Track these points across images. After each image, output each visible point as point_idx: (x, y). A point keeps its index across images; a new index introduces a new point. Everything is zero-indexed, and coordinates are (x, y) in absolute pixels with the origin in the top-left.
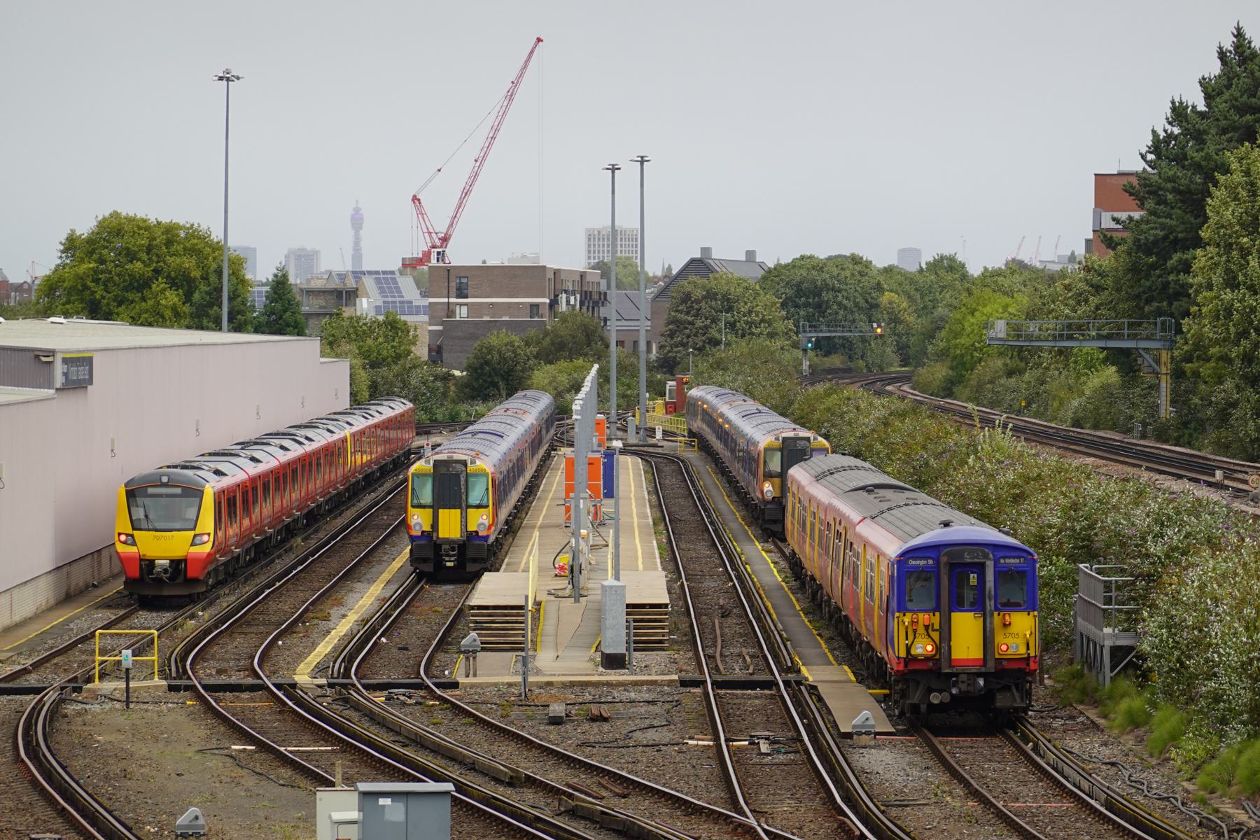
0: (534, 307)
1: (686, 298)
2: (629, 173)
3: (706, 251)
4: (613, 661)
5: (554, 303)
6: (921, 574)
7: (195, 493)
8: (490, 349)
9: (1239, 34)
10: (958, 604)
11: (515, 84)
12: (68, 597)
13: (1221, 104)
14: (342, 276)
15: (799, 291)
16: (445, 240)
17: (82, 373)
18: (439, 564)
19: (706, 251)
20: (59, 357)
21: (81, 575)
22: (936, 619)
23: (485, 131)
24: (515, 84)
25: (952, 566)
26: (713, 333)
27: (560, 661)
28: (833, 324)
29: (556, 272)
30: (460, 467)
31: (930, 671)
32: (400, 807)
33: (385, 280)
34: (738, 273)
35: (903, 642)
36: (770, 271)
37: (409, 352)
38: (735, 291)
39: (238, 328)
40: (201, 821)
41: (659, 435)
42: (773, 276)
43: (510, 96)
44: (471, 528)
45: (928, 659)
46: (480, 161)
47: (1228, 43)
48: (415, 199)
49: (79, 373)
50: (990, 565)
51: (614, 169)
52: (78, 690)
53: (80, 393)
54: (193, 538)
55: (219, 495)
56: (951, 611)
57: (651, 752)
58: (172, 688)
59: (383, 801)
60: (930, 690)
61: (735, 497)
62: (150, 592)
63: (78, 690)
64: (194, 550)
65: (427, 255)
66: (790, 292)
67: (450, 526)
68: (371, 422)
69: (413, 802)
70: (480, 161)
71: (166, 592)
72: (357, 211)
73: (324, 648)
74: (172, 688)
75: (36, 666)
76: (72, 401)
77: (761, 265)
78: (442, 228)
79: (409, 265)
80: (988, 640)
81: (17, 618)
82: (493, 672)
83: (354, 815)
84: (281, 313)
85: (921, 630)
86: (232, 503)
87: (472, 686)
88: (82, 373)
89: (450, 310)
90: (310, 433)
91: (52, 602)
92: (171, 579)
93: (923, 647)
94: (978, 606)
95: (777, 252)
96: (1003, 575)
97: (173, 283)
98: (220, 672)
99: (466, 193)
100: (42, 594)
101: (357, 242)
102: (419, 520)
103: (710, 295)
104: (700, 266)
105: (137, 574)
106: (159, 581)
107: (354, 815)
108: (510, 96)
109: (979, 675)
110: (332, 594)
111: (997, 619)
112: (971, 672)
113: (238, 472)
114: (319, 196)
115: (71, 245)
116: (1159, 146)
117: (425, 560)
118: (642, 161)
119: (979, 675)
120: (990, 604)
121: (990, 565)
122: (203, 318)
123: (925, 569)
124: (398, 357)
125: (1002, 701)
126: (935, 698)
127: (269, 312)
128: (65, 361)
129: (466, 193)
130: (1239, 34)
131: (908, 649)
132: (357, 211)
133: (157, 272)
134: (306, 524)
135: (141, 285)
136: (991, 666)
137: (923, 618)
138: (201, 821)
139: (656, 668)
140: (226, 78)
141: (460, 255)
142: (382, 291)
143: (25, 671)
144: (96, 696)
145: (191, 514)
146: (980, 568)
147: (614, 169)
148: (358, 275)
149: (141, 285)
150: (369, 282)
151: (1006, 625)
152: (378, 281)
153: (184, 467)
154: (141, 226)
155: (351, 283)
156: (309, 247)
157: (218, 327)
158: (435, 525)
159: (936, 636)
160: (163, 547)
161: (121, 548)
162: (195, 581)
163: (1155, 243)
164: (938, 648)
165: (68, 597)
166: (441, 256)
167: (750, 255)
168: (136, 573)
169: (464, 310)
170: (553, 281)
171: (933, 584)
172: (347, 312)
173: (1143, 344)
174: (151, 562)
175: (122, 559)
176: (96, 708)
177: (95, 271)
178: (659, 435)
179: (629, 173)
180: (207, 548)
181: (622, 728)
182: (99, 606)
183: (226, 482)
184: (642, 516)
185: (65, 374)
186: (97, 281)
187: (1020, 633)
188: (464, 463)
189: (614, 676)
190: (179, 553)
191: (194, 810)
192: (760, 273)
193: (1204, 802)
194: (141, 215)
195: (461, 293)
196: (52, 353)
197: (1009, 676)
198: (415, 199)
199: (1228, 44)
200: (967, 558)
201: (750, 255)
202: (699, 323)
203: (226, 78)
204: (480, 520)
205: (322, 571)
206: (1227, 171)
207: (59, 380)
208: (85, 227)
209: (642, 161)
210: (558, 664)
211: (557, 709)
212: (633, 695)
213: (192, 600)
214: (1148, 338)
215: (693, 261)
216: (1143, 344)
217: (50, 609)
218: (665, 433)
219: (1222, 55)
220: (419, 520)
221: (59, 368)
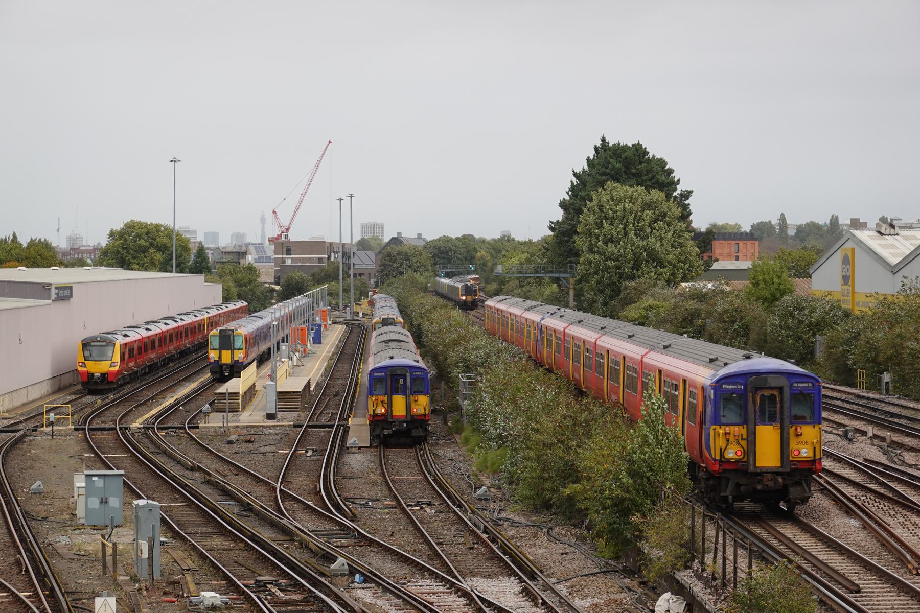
0: (320, 259)
1: (389, 255)
2: (346, 203)
3: (399, 234)
4: (270, 417)
5: (329, 258)
6: (380, 380)
8: (292, 278)
9: (603, 140)
10: (395, 391)
12: (59, 390)
13: (594, 172)
14: (240, 246)
15: (441, 252)
16: (288, 229)
17: (67, 293)
18: (222, 373)
20: (53, 287)
21: (66, 380)
22: (386, 399)
23: (305, 182)
24: (319, 161)
25: (392, 376)
26: (401, 269)
27: (251, 417)
29: (331, 244)
30: (230, 332)
31: (383, 421)
32: (101, 481)
33: (259, 247)
34: (414, 243)
35: (372, 408)
36: (427, 243)
37: (255, 280)
39: (181, 271)
40: (42, 487)
41: (361, 315)
42: (429, 245)
43: (317, 166)
45: (382, 415)
46: (303, 195)
47: (599, 143)
48: (274, 212)
49: (65, 293)
50: (408, 375)
51: (341, 200)
52: (36, 430)
53: (66, 302)
54: (109, 363)
56: (392, 395)
57: (261, 456)
58: (76, 429)
59: (94, 478)
60: (384, 429)
62: (94, 387)
63: (36, 430)
64: (111, 369)
65: (280, 236)
66: (436, 251)
70: (303, 195)
71: (99, 388)
74: (76, 429)
75: (26, 420)
76: (61, 306)
77: (424, 240)
78: (286, 224)
80: (408, 407)
81: (30, 399)
82: (215, 421)
83: (84, 484)
85: (380, 403)
86: (129, 351)
87: (205, 427)
88: (67, 293)
89: (283, 261)
90: (183, 317)
91: (50, 392)
94: (404, 393)
95: (431, 235)
98: (102, 422)
99: (297, 209)
100: (45, 388)
101: (263, 230)
102: (213, 355)
103: (399, 254)
104: (396, 240)
105: (86, 379)
106: (96, 383)
107: (84, 484)
108: (317, 166)
109: (404, 422)
110: (171, 388)
111: (412, 398)
113: (134, 336)
115: (112, 234)
117: (216, 373)
118: (351, 197)
119: (404, 422)
120: (408, 392)
121: (408, 375)
122: (165, 267)
123: (380, 377)
124: (251, 282)
125: (415, 433)
126: (386, 432)
127: (196, 262)
128: (56, 288)
129: (297, 209)
131: (374, 411)
133: (151, 245)
134: (174, 356)
136: (409, 419)
138: (42, 487)
139: (287, 419)
140: (174, 161)
141: (294, 237)
142: (257, 252)
143: (20, 422)
144: (42, 432)
145: (110, 354)
146: (404, 376)
147: (341, 200)
148: (247, 245)
149: (145, 250)
150: (252, 248)
152: (256, 248)
153: (110, 333)
154: (142, 225)
155: (244, 249)
157: (171, 272)
159: (386, 405)
160: (98, 368)
161: (80, 369)
162: (112, 382)
163: (566, 231)
164: (386, 411)
165: (59, 390)
166: (286, 237)
167: (419, 235)
168: (86, 379)
169: (290, 260)
170: (331, 248)
171: (384, 384)
172: (242, 262)
173: (562, 275)
174: (93, 374)
175: (82, 373)
176: (40, 438)
177: (122, 244)
178: (361, 315)
179: (346, 203)
180: (117, 368)
181: (256, 445)
182: (71, 394)
183: (128, 340)
185: (57, 294)
186: (124, 249)
187: (421, 405)
188: (233, 331)
190: (105, 370)
191: (39, 482)
193: (476, 476)
194: (143, 220)
196: (50, 285)
198: (274, 212)
200: (399, 373)
201: (419, 235)
202: (395, 265)
203: (174, 161)
204: (239, 355)
206: (591, 200)
207: (53, 296)
208: (118, 226)
209: (351, 197)
210: (251, 418)
211: (233, 438)
212: (272, 431)
213: (110, 391)
214: (564, 272)
215: (393, 238)
216: (562, 275)
217: (50, 395)
218: (364, 314)
219: (596, 148)
220: (213, 355)
221: (53, 291)
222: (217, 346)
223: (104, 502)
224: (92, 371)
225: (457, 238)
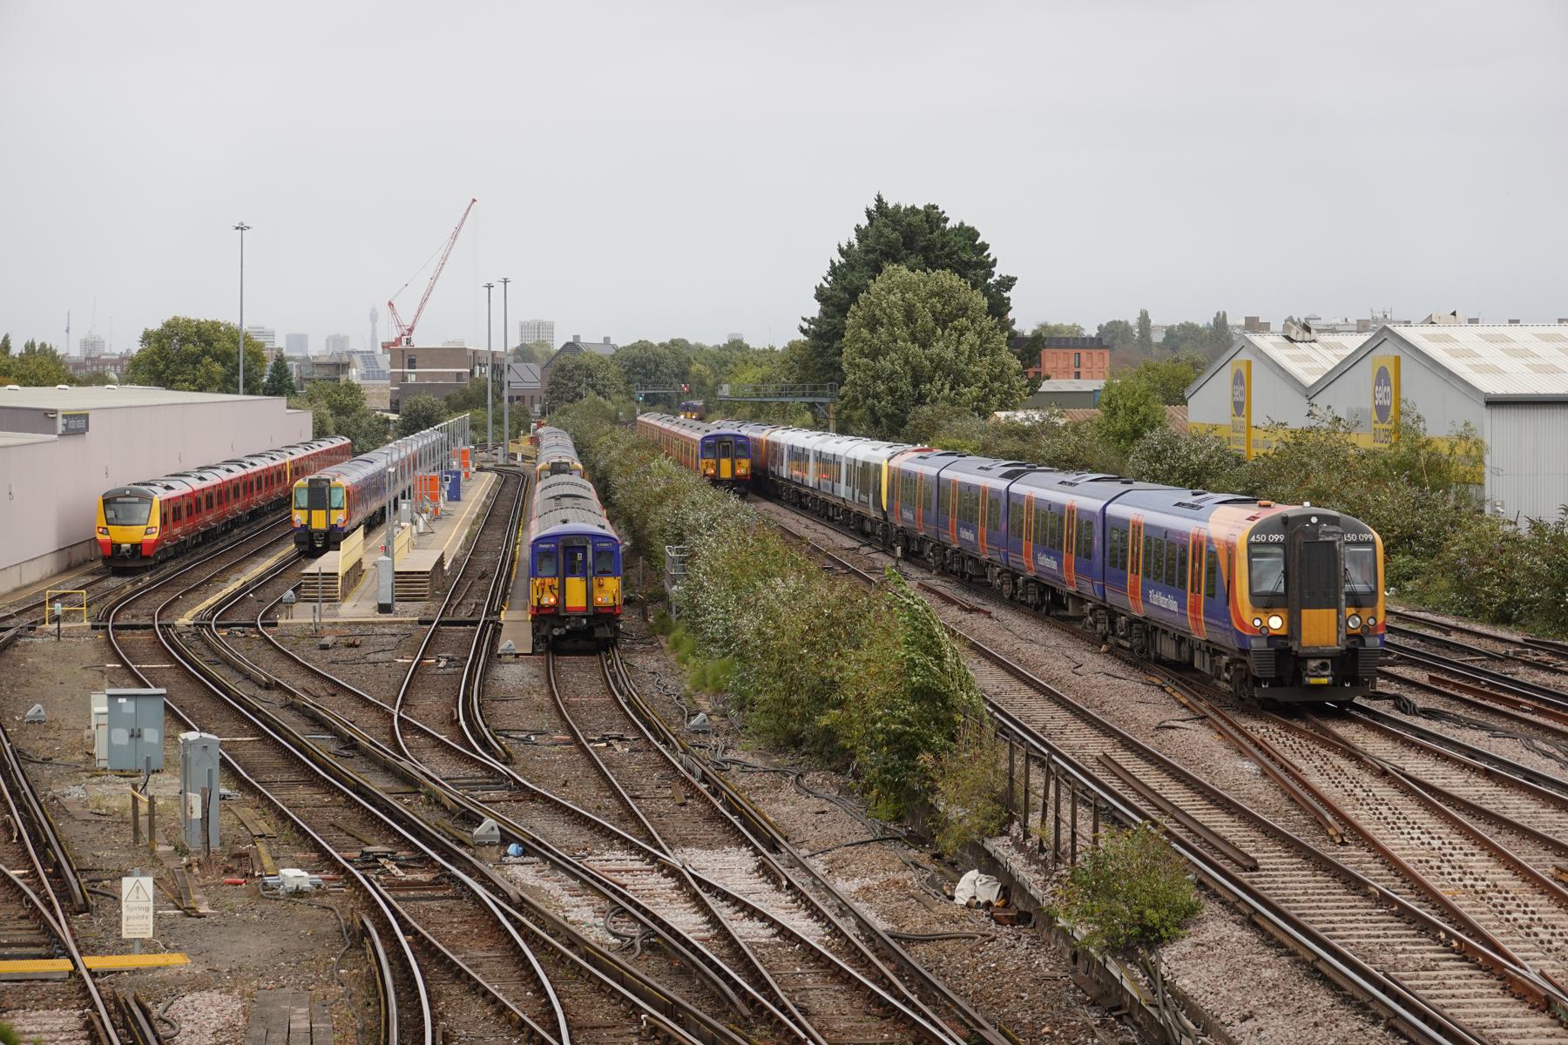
0: (459, 374)
2: (498, 290)
3: (576, 337)
4: (384, 609)
5: (472, 373)
6: (547, 554)
7: (146, 499)
9: (879, 200)
10: (572, 573)
11: (458, 229)
14: (340, 355)
15: (635, 365)
16: (410, 330)
17: (80, 424)
19: (576, 337)
21: (79, 554)
22: (556, 582)
24: (458, 229)
25: (566, 548)
28: (656, 383)
29: (474, 352)
32: (132, 703)
33: (369, 357)
35: (536, 597)
38: (593, 364)
39: (252, 392)
43: (455, 236)
44: (333, 522)
45: (551, 607)
46: (434, 279)
50: (590, 547)
51: (489, 286)
54: (145, 529)
55: (165, 503)
58: (94, 627)
59: (121, 700)
61: (491, 502)
65: (399, 340)
67: (319, 521)
68: (311, 452)
69: (140, 701)
70: (434, 279)
71: (129, 565)
72: (374, 310)
73: (210, 601)
74: (94, 627)
76: (72, 443)
78: (409, 323)
79: (386, 346)
81: (26, 582)
83: (105, 709)
84: (279, 383)
88: (80, 424)
89: (404, 377)
90: (255, 461)
92: (133, 556)
93: (549, 600)
94: (584, 574)
95: (624, 338)
96: (598, 554)
97: (216, 358)
100: (48, 566)
102: (299, 517)
103: (578, 367)
106: (124, 558)
107: (105, 709)
108: (455, 236)
110: (237, 566)
111: (595, 581)
112: (578, 615)
113: (181, 488)
114: (308, 307)
115: (147, 337)
116: (834, 270)
118: (505, 282)
120: (590, 572)
121: (590, 547)
126: (556, 632)
130: (879, 200)
132: (374, 310)
134: (242, 519)
135: (195, 360)
137: (548, 581)
139: (409, 612)
140: (241, 228)
141: (420, 341)
142: (365, 364)
143: (11, 617)
144: (42, 632)
147: (489, 286)
148: (350, 353)
149: (195, 360)
150: (357, 359)
151: (601, 586)
155: (345, 359)
156: (546, 319)
158: (309, 521)
160: (127, 536)
161: (99, 537)
162: (148, 557)
165: (69, 568)
167: (607, 340)
170: (475, 358)
172: (343, 378)
174: (119, 546)
176: (39, 640)
179: (498, 290)
180: (155, 536)
181: (363, 651)
183: (171, 494)
184: (471, 513)
185: (66, 425)
187: (610, 590)
189: (384, 618)
191: (38, 706)
192: (613, 352)
195: (412, 364)
196: (55, 411)
197: (603, 617)
199: (872, 207)
201: (607, 340)
203: (241, 228)
204: (338, 517)
205: (243, 549)
207: (60, 429)
208: (156, 326)
209: (505, 282)
211: (328, 640)
213: (145, 569)
218: (524, 457)
219: (869, 213)
220: (299, 517)
221: (60, 422)
222: (305, 504)
223: (136, 735)
224: (118, 540)
225: (662, 345)
